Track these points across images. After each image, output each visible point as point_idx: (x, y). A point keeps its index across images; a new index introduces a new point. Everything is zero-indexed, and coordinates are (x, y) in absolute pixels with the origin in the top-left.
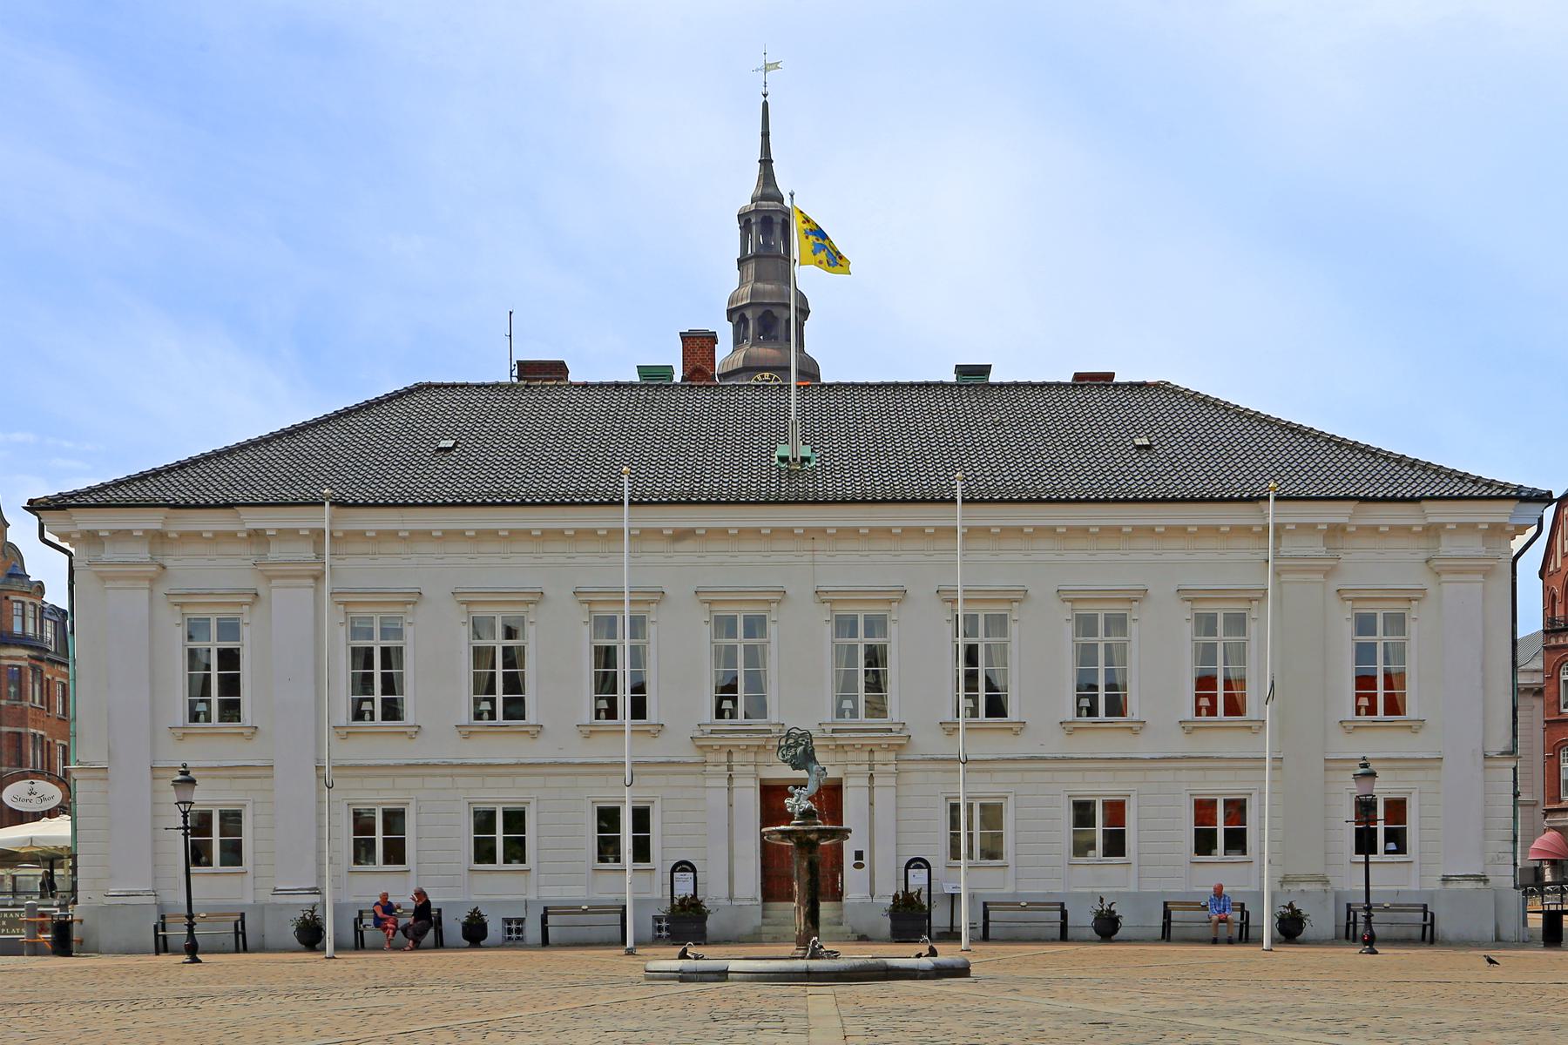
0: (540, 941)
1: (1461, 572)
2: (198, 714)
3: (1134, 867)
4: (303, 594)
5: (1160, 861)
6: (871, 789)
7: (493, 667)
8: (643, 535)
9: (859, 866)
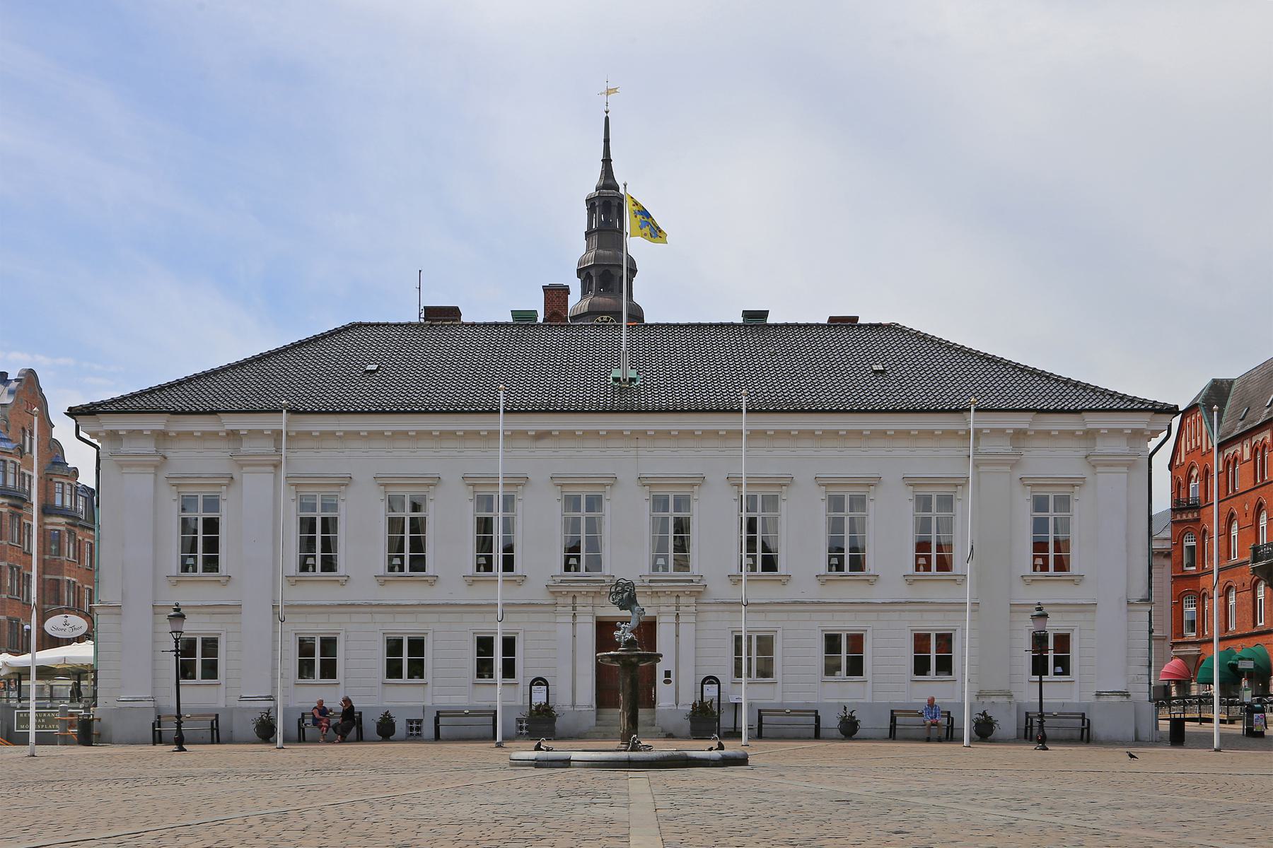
6: (677, 624)
8: (513, 436)
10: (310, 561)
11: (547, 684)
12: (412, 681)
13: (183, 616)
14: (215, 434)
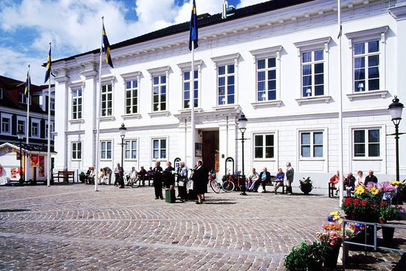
4: (63, 86)
12: (315, 158)
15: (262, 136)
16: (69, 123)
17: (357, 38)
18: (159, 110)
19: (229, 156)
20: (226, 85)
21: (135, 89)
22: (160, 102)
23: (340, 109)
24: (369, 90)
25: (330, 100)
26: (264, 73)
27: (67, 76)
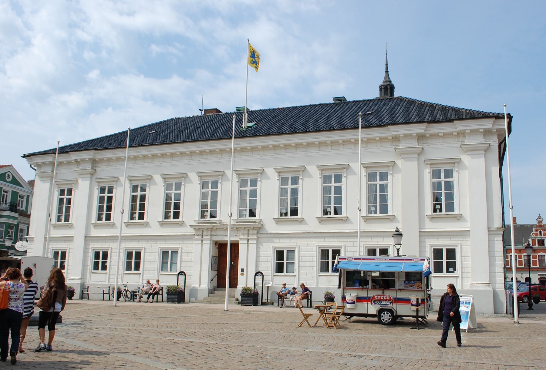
0: (492, 311)
1: (475, 150)
2: (436, 209)
3: (297, 277)
4: (47, 185)
5: (150, 273)
6: (202, 244)
7: (330, 194)
8: (369, 141)
9: (242, 274)
10: (244, 212)
11: (185, 275)
12: (288, 274)
13: (401, 235)
14: (451, 134)
15: (376, 250)
16: (124, 225)
17: (243, 174)
18: (104, 221)
19: (182, 270)
20: (138, 203)
21: (69, 197)
22: (64, 214)
23: (119, 232)
24: (380, 213)
25: (346, 220)
26: (104, 197)
27: (93, 168)
